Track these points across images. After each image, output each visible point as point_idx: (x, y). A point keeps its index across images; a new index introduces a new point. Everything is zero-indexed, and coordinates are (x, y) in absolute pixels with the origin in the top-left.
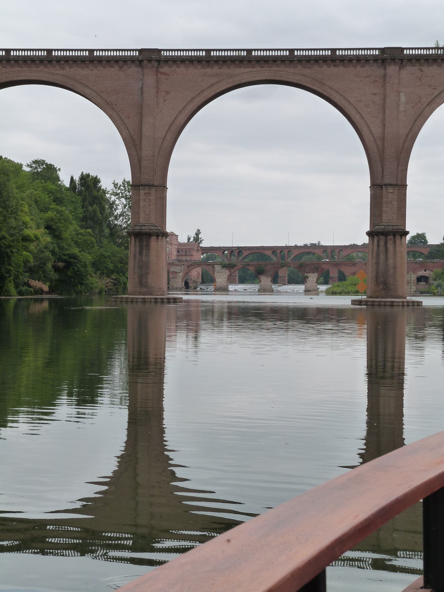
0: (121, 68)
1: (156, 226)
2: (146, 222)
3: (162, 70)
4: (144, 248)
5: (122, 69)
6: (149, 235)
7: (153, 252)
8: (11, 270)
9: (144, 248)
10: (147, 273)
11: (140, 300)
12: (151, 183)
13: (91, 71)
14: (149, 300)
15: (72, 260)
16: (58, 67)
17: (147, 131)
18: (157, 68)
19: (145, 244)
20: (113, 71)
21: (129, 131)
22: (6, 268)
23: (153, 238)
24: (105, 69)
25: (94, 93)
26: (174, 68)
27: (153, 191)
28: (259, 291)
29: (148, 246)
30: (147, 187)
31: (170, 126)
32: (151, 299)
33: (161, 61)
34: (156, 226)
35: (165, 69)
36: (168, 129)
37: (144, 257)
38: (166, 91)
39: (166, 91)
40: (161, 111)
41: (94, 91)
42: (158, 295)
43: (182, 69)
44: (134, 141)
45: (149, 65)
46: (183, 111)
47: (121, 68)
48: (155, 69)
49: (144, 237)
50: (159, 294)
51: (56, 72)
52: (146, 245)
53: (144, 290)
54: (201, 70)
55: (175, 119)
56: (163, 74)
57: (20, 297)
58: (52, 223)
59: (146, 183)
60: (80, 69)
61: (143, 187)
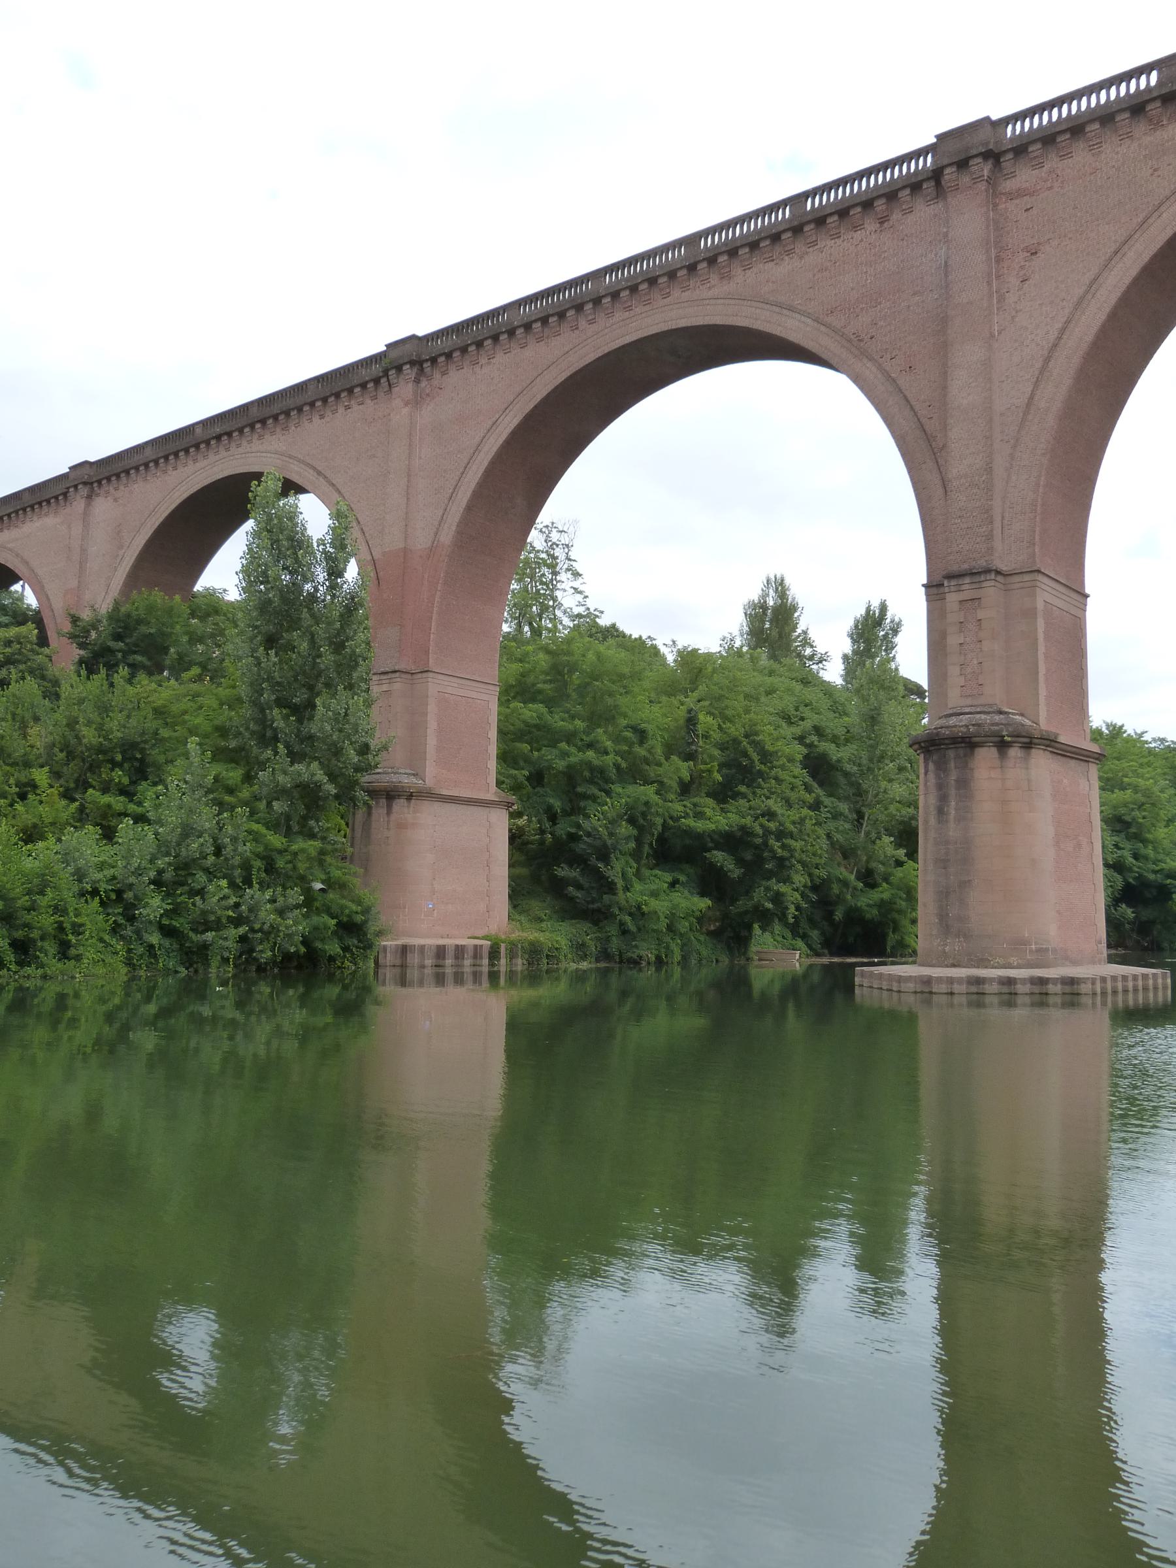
0: (882, 221)
1: (1001, 712)
2: (969, 701)
3: (1008, 185)
4: (953, 792)
5: (886, 225)
6: (967, 743)
7: (984, 807)
8: (783, 895)
9: (953, 792)
10: (964, 885)
11: (911, 986)
12: (982, 563)
13: (801, 258)
14: (943, 988)
15: (1169, 881)
16: (714, 278)
17: (964, 392)
18: (991, 182)
19: (953, 776)
20: (866, 234)
21: (912, 408)
22: (768, 889)
23: (986, 756)
24: (839, 241)
25: (809, 320)
26: (1052, 161)
27: (991, 590)
28: (1078, 984)
29: (964, 784)
30: (967, 580)
31: (1047, 360)
32: (951, 980)
33: (1005, 152)
34: (1001, 712)
35: (1023, 176)
36: (1041, 373)
37: (952, 825)
38: (1026, 249)
39: (1026, 249)
40: (1013, 318)
41: (809, 316)
42: (1010, 967)
43: (1081, 155)
44: (929, 438)
45: (966, 179)
46: (1089, 296)
47: (882, 221)
48: (982, 186)
49: (951, 754)
50: (1014, 960)
51: (710, 294)
52: (957, 781)
53: (954, 946)
54: (1148, 139)
55: (1063, 331)
56: (1011, 196)
57: (836, 960)
58: (1123, 811)
59: (966, 566)
60: (771, 264)
61: (953, 582)
